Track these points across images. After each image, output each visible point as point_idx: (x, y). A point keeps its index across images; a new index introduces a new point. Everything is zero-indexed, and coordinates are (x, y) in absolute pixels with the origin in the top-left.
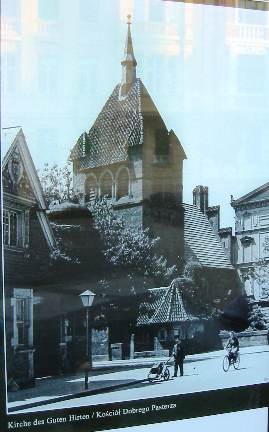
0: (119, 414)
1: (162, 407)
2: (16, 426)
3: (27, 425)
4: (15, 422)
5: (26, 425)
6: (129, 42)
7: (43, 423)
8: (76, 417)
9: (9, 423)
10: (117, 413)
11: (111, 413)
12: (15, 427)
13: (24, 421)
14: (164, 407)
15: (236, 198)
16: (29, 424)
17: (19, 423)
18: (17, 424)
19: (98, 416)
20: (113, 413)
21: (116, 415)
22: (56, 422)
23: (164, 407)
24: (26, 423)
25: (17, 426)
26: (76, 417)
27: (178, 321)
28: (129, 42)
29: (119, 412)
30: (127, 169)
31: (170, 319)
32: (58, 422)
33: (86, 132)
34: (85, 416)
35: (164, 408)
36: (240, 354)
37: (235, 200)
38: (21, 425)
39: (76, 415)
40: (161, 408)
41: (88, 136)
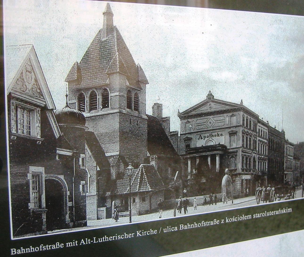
0: (243, 219)
1: (46, 248)
2: (144, 234)
3: (128, 237)
4: (143, 230)
7: (119, 236)
8: (170, 228)
9: (138, 232)
10: (241, 219)
11: (237, 218)
12: (143, 235)
15: (181, 111)
16: (156, 232)
17: (146, 232)
18: (145, 232)
19: (139, 235)
20: (238, 218)
21: (36, 251)
22: (101, 241)
24: (127, 235)
25: (145, 235)
26: (170, 228)
29: (242, 217)
31: (139, 190)
33: (77, 62)
35: (171, 230)
37: (180, 112)
39: (143, 230)
40: (45, 249)
41: (79, 65)
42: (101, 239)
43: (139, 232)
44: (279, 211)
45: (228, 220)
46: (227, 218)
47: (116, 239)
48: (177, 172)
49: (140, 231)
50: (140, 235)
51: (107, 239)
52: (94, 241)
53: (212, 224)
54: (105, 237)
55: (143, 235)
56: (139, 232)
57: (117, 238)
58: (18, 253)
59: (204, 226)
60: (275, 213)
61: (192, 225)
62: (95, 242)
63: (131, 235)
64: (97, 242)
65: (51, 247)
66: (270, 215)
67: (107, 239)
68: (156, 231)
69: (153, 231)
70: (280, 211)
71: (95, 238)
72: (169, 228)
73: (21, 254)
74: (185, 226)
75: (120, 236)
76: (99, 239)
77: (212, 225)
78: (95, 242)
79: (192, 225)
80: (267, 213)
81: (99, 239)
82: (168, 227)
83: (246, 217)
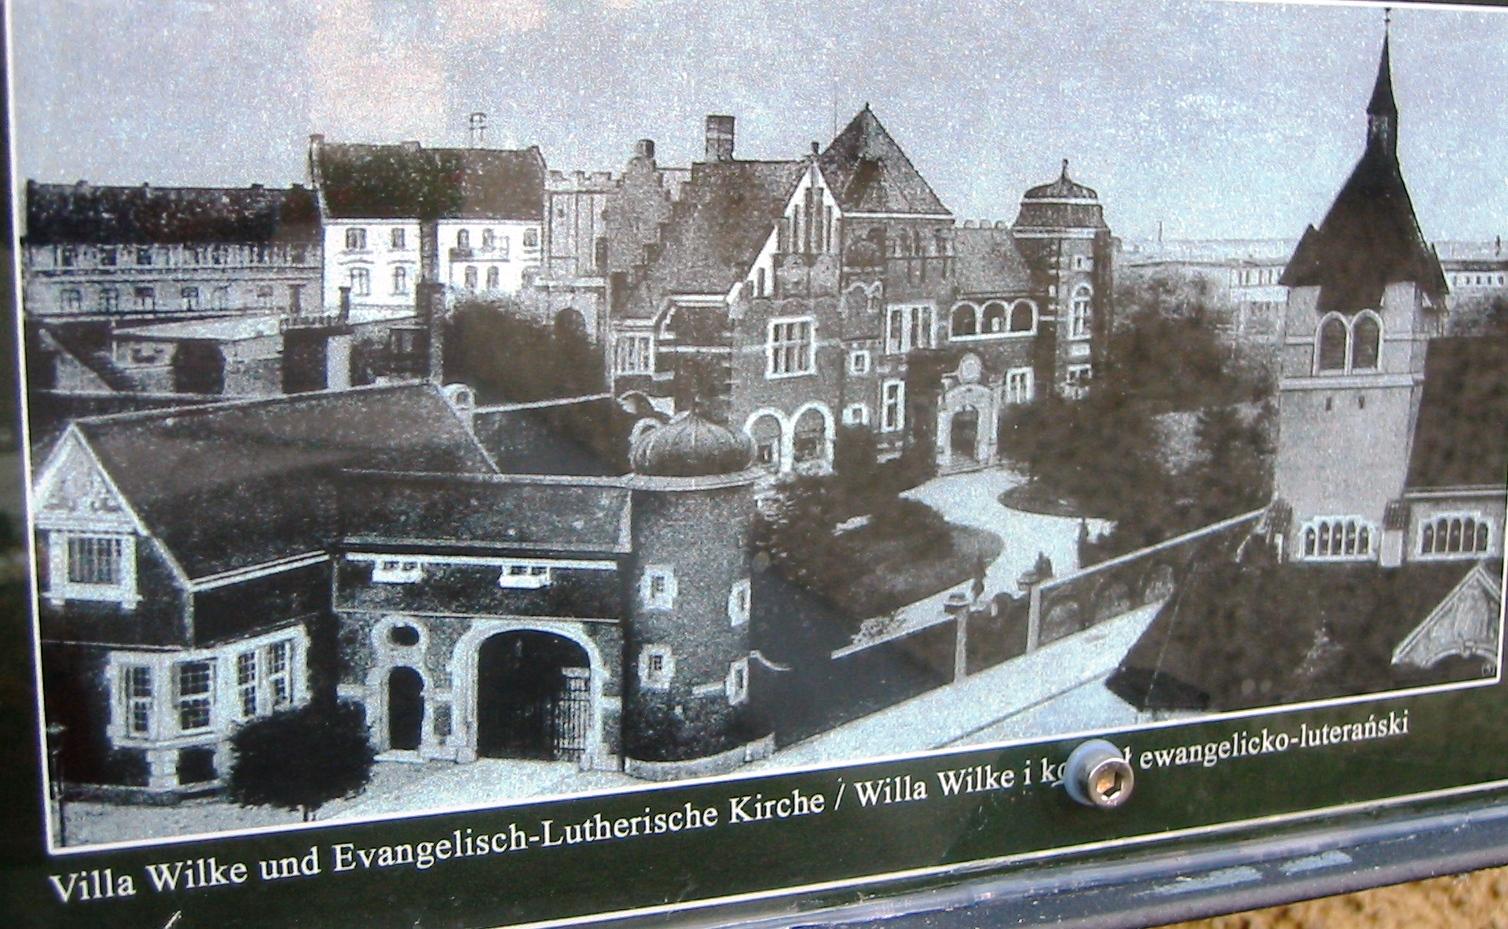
2: (764, 813)
3: (702, 822)
4: (759, 796)
5: (296, 872)
6: (1382, 104)
9: (734, 801)
12: (759, 817)
13: (598, 817)
14: (1328, 734)
16: (818, 806)
17: (774, 802)
18: (768, 804)
19: (738, 816)
21: (307, 872)
22: (578, 839)
23: (1328, 734)
24: (804, 799)
25: (768, 815)
26: (469, 841)
27: (549, 185)
28: (1382, 104)
30: (1371, 313)
32: (589, 838)
34: (626, 824)
35: (1328, 737)
36: (455, 245)
38: (784, 808)
42: (578, 827)
43: (742, 805)
44: (1367, 726)
45: (1273, 743)
46: (1045, 761)
47: (648, 831)
48: (837, 654)
49: (746, 799)
50: (747, 818)
51: (603, 828)
52: (542, 840)
53: (1357, 736)
54: (594, 821)
55: (759, 817)
56: (742, 805)
57: (652, 829)
58: (121, 892)
59: (479, 852)
60: (1350, 733)
61: (1192, 749)
62: (547, 843)
63: (1150, 756)
64: (560, 842)
65: (637, 824)
66: (1325, 742)
67: (603, 828)
68: (1012, 775)
69: (697, 813)
70: (1371, 724)
71: (547, 824)
72: (462, 839)
73: (1364, 740)
74: (916, 786)
75: (664, 816)
76: (568, 829)
77: (1183, 765)
78: (547, 843)
79: (1192, 749)
80: (1311, 733)
81: (568, 829)
82: (1236, 736)
83: (1339, 731)
